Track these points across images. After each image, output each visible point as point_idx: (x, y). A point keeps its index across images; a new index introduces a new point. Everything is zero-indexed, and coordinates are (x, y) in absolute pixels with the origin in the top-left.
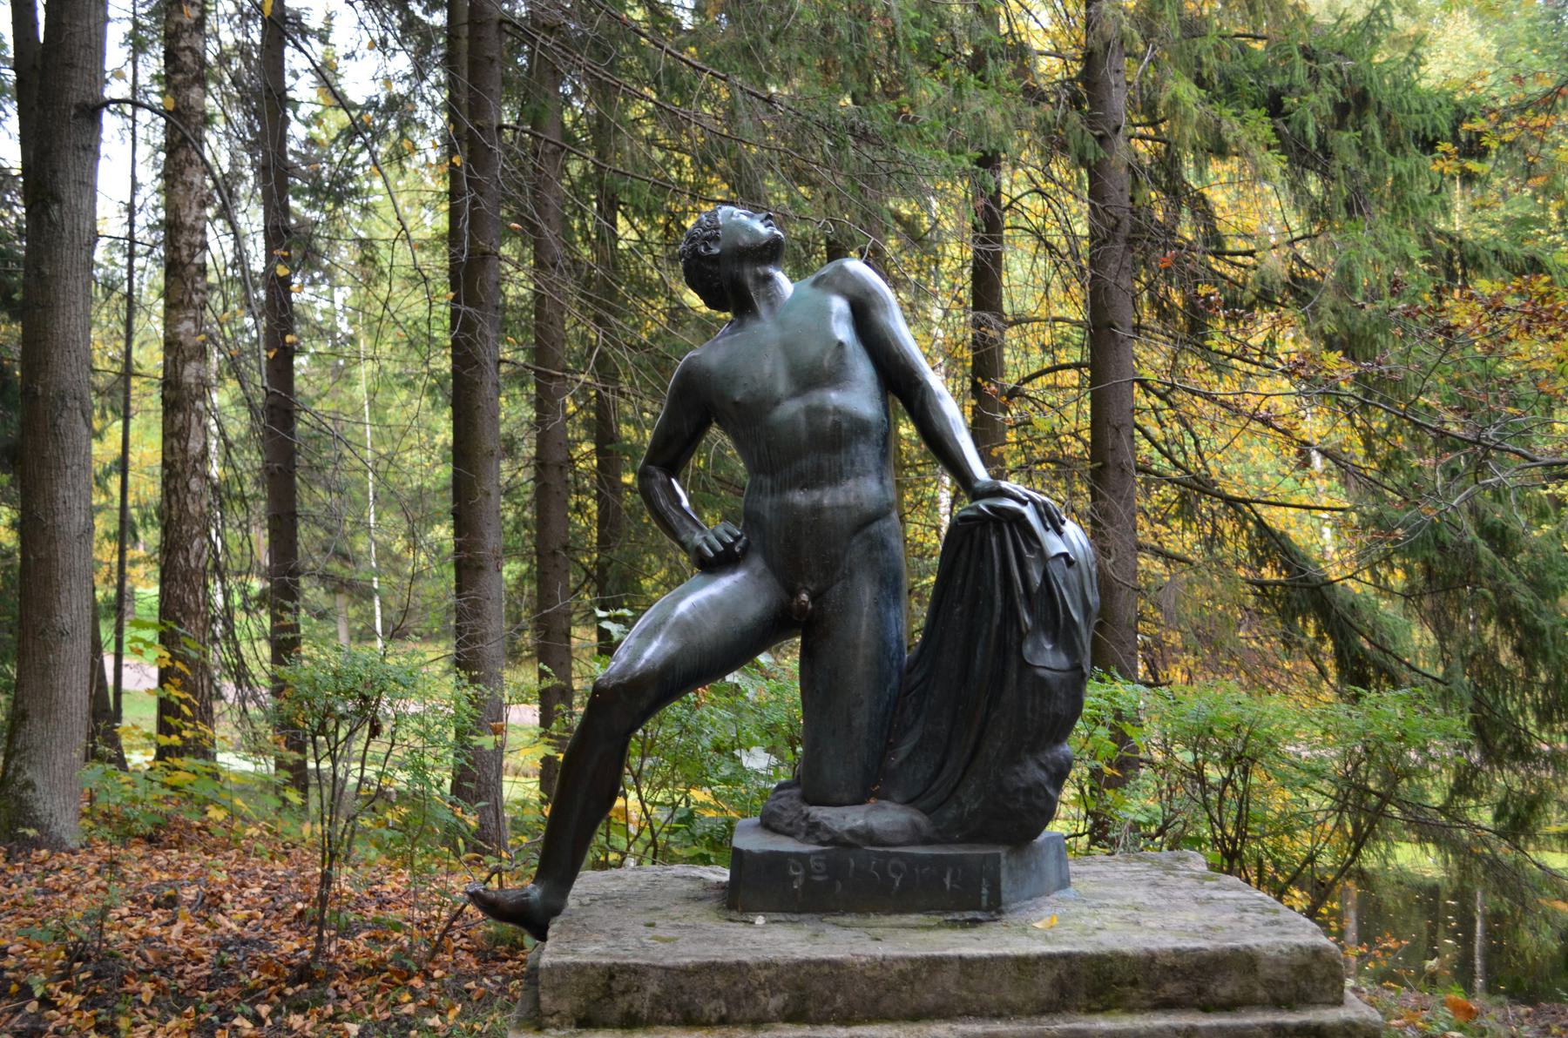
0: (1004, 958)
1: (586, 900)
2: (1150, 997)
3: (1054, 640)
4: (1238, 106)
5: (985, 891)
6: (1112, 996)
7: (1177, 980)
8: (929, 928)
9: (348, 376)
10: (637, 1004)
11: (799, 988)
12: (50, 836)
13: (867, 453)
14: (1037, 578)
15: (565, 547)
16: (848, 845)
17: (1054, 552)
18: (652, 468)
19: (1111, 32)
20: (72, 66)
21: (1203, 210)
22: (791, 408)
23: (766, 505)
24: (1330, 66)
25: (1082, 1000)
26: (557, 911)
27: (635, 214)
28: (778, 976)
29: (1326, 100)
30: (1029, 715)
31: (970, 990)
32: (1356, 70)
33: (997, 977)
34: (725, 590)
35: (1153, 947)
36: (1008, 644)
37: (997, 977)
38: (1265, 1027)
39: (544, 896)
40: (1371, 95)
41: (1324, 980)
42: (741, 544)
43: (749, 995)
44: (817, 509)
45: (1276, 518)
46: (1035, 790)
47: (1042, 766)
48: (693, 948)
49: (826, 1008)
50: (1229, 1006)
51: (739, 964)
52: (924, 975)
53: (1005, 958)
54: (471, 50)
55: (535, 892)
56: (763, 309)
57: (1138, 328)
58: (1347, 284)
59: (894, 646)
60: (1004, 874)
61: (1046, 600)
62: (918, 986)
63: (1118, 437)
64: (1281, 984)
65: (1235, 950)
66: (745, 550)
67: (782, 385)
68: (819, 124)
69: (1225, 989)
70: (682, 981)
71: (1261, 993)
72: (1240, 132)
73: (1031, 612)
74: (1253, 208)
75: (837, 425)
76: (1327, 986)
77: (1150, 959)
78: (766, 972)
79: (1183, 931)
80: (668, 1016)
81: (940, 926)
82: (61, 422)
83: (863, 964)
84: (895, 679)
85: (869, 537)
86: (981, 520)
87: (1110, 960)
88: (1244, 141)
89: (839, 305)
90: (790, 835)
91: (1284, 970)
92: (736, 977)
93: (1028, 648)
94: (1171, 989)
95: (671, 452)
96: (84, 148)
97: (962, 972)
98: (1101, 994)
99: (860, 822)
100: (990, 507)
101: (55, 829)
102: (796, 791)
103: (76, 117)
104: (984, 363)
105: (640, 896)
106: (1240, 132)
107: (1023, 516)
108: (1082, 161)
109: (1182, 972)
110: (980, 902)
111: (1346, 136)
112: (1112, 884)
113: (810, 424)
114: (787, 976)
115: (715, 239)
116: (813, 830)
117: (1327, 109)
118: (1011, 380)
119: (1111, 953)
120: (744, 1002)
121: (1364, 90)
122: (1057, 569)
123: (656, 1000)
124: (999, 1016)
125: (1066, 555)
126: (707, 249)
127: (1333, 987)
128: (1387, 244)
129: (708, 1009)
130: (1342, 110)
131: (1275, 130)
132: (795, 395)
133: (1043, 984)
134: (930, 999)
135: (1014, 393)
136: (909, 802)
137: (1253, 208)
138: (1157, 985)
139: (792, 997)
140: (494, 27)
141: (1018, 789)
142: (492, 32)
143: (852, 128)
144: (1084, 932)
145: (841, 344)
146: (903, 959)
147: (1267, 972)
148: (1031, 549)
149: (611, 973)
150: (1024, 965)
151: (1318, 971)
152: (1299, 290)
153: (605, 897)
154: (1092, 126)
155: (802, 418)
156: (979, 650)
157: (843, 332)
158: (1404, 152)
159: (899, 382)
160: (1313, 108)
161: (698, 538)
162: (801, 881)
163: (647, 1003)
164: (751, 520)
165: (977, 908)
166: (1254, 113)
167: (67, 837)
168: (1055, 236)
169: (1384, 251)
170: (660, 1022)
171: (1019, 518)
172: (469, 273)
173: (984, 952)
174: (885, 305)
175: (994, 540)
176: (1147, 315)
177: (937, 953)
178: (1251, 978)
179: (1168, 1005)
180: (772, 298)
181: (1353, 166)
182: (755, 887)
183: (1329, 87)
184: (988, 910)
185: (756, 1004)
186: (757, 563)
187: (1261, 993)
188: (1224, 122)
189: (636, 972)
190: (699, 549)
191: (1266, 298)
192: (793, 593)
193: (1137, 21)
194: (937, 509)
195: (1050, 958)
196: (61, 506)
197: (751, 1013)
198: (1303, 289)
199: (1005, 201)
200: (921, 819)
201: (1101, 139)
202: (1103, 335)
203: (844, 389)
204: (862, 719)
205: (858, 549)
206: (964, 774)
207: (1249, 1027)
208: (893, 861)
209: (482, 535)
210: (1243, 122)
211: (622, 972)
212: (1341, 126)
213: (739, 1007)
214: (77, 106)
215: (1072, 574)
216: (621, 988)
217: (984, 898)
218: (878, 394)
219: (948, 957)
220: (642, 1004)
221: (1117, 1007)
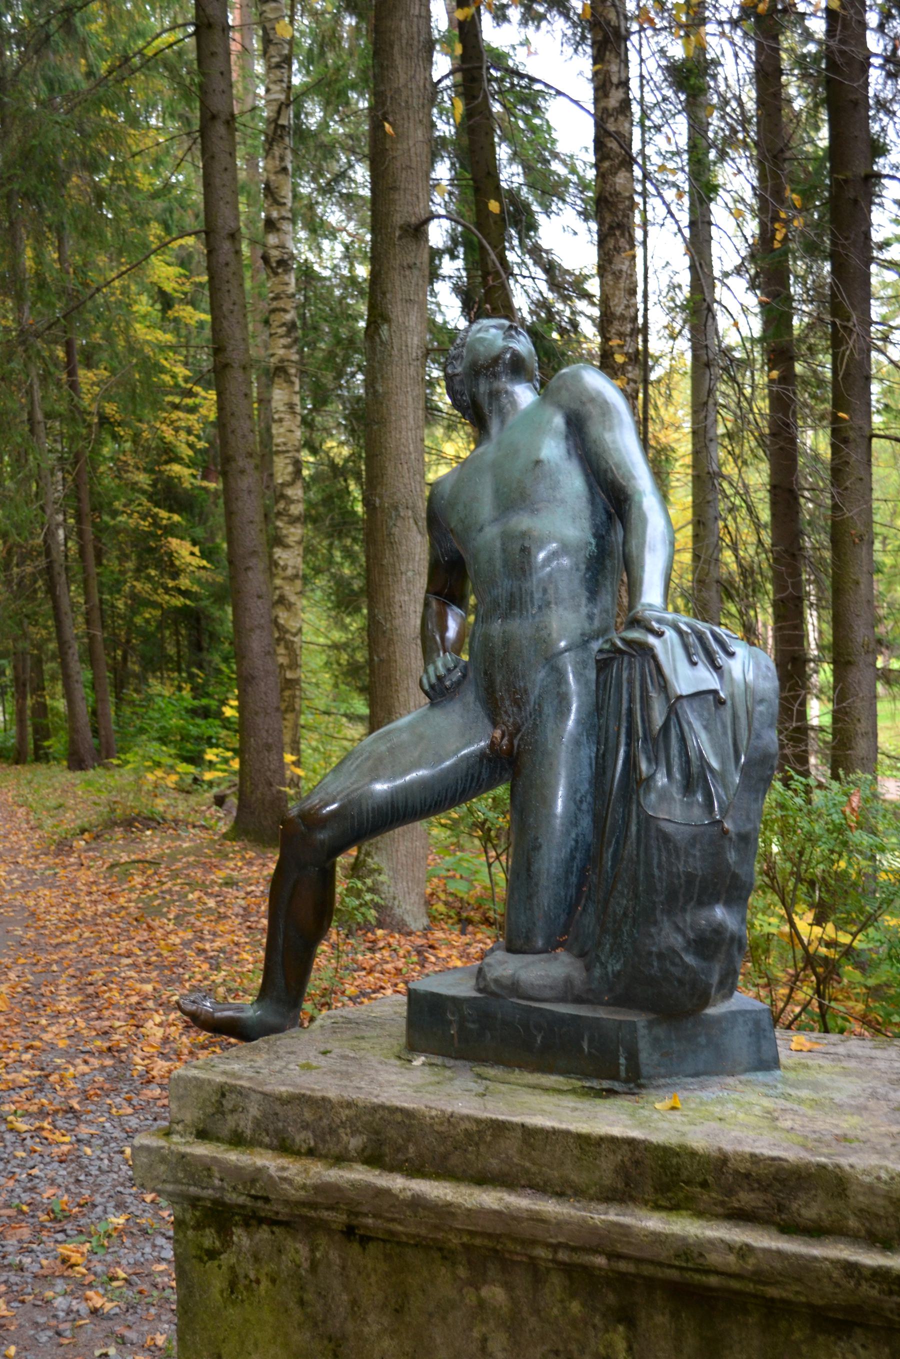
2: (723, 1203)
5: (622, 1061)
6: (681, 1195)
7: (753, 1190)
8: (560, 1091)
10: (242, 1123)
11: (377, 1133)
12: (393, 916)
14: (658, 718)
20: (395, 189)
25: (650, 1195)
30: (656, 872)
33: (558, 1153)
35: (728, 1148)
37: (558, 1153)
38: (835, 1262)
43: (332, 1131)
47: (678, 929)
49: (400, 1156)
50: (815, 1231)
51: (324, 1099)
52: (489, 1139)
62: (483, 1149)
64: (878, 1217)
65: (822, 1167)
69: (811, 1210)
70: (278, 1108)
71: (853, 1223)
77: (722, 1161)
78: (347, 1112)
80: (267, 1140)
81: (573, 1091)
82: (396, 531)
83: (432, 1118)
87: (678, 1155)
91: (880, 1202)
92: (322, 1112)
94: (746, 1198)
96: (410, 267)
97: (525, 1141)
98: (669, 1190)
101: (398, 911)
103: (400, 238)
109: (758, 1181)
110: (618, 1072)
114: (364, 1118)
119: (680, 1147)
120: (328, 1138)
124: (560, 1195)
125: (715, 692)
132: (496, 520)
134: (494, 1164)
138: (730, 1192)
139: (369, 1140)
146: (468, 1118)
149: (223, 1091)
155: (498, 544)
163: (250, 1125)
165: (615, 1077)
167: (408, 919)
170: (261, 1144)
177: (501, 1117)
178: (841, 1204)
184: (627, 1081)
185: (339, 1142)
187: (853, 1223)
189: (240, 1093)
196: (397, 610)
197: (336, 1150)
207: (815, 1259)
209: (851, 627)
211: (231, 1092)
214: (401, 228)
216: (230, 1107)
217: (622, 1068)
219: (511, 1123)
221: (687, 1209)
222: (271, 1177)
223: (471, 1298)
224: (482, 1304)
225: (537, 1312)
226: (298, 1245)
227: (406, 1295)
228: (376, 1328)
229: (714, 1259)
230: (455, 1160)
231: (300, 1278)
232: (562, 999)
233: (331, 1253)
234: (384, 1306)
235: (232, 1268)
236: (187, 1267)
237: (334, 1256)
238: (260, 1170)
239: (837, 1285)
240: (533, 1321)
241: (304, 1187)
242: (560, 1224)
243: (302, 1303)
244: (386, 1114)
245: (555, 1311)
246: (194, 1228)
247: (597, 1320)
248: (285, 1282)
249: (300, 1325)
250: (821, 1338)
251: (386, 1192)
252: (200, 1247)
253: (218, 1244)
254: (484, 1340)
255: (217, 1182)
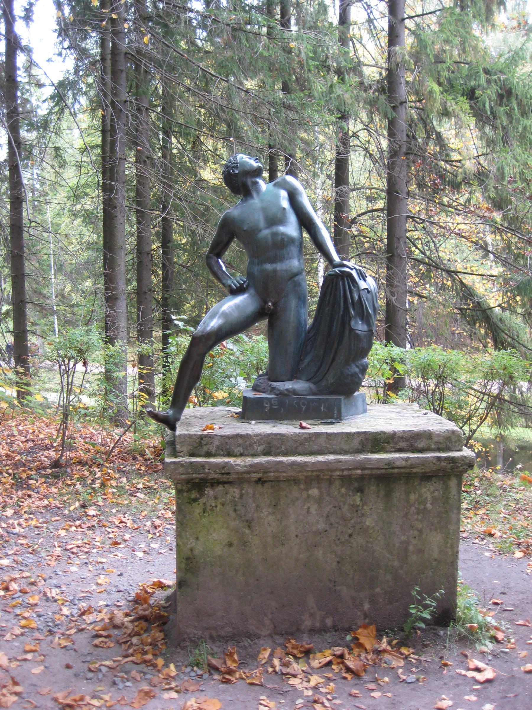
0: (342, 433)
1: (188, 417)
3: (362, 320)
4: (455, 95)
9: (40, 210)
10: (211, 448)
11: (269, 443)
13: (294, 250)
14: (356, 297)
15: (150, 290)
16: (286, 395)
17: (363, 288)
18: (211, 255)
19: (399, 60)
21: (439, 139)
22: (266, 233)
23: (256, 270)
24: (496, 77)
26: (178, 420)
27: (181, 136)
28: (261, 439)
29: (493, 93)
31: (330, 445)
32: (507, 79)
34: (241, 301)
35: (396, 430)
36: (346, 319)
37: (339, 440)
39: (173, 414)
40: (513, 91)
41: (456, 442)
42: (246, 284)
43: (250, 445)
44: (275, 271)
45: (468, 280)
46: (354, 375)
47: (357, 367)
48: (230, 430)
49: (278, 451)
51: (247, 434)
53: (343, 433)
54: (113, 65)
55: (171, 412)
56: (255, 195)
57: (408, 193)
58: (501, 176)
59: (303, 322)
60: (343, 406)
61: (360, 305)
62: (311, 443)
63: (399, 243)
64: (441, 443)
65: (425, 431)
66: (248, 286)
67: (262, 224)
68: (269, 102)
70: (227, 440)
72: (455, 107)
73: (354, 310)
74: (463, 140)
75: (283, 239)
76: (457, 444)
79: (407, 425)
81: (319, 424)
84: (303, 335)
85: (294, 281)
86: (336, 275)
87: (380, 434)
88: (457, 111)
89: (284, 194)
90: (264, 392)
93: (353, 323)
94: (402, 444)
95: (218, 248)
97: (327, 438)
99: (290, 387)
100: (339, 271)
102: (266, 377)
104: (340, 207)
105: (207, 416)
106: (455, 107)
107: (351, 274)
108: (386, 116)
111: (502, 109)
112: (383, 412)
113: (273, 239)
115: (236, 167)
116: (273, 389)
117: (494, 97)
118: (353, 215)
121: (511, 88)
122: (364, 294)
123: (218, 447)
125: (367, 289)
126: (233, 171)
127: (459, 445)
128: (519, 158)
129: (236, 450)
130: (501, 97)
131: (471, 106)
132: (267, 228)
133: (356, 443)
134: (315, 448)
135: (354, 221)
136: (308, 380)
137: (463, 140)
138: (396, 443)
140: (122, 56)
141: (348, 375)
142: (122, 58)
143: (283, 104)
144: (371, 426)
145: (284, 209)
147: (436, 439)
148: (354, 287)
149: (202, 438)
150: (349, 436)
151: (454, 439)
152: (481, 176)
153: (194, 416)
154: (390, 102)
155: (270, 237)
156: (335, 324)
157: (285, 204)
158: (527, 116)
159: (305, 222)
160: (488, 95)
161: (229, 282)
162: (268, 408)
163: (214, 448)
164: (250, 275)
166: (461, 99)
168: (373, 148)
169: (517, 161)
171: (350, 275)
172: (109, 168)
173: (335, 431)
174: (301, 194)
175: (341, 283)
176: (413, 187)
178: (430, 441)
179: (400, 450)
180: (258, 190)
181: (505, 123)
182: (251, 409)
183: (495, 87)
184: (336, 419)
185: (253, 449)
186: (252, 291)
188: (448, 102)
190: (230, 286)
191: (466, 181)
192: (266, 302)
193: (411, 55)
194: (317, 274)
195: (359, 433)
197: (252, 452)
198: (481, 178)
199: (351, 133)
200: (312, 386)
201: (394, 108)
202: (393, 195)
203: (285, 226)
204: (291, 349)
205: (290, 285)
206: (328, 370)
208: (302, 401)
209: (117, 284)
210: (456, 103)
212: (501, 105)
213: (247, 450)
215: (369, 296)
218: (298, 228)
220: (213, 449)
222: (232, 465)
223: (305, 495)
224: (309, 496)
225: (329, 495)
226: (235, 490)
227: (279, 499)
228: (266, 513)
229: (398, 463)
230: (300, 449)
231: (235, 502)
232: (309, 395)
233: (249, 490)
234: (270, 505)
235: (205, 504)
236: (183, 507)
237: (251, 491)
238: (226, 463)
239: (435, 464)
240: (328, 498)
241: (245, 466)
242: (346, 462)
243: (235, 510)
244: (273, 437)
245: (336, 493)
246: (187, 492)
247: (351, 493)
248: (228, 504)
249: (234, 519)
250: (423, 483)
251: (281, 462)
252: (189, 499)
253: (198, 496)
254: (309, 508)
255: (207, 471)
